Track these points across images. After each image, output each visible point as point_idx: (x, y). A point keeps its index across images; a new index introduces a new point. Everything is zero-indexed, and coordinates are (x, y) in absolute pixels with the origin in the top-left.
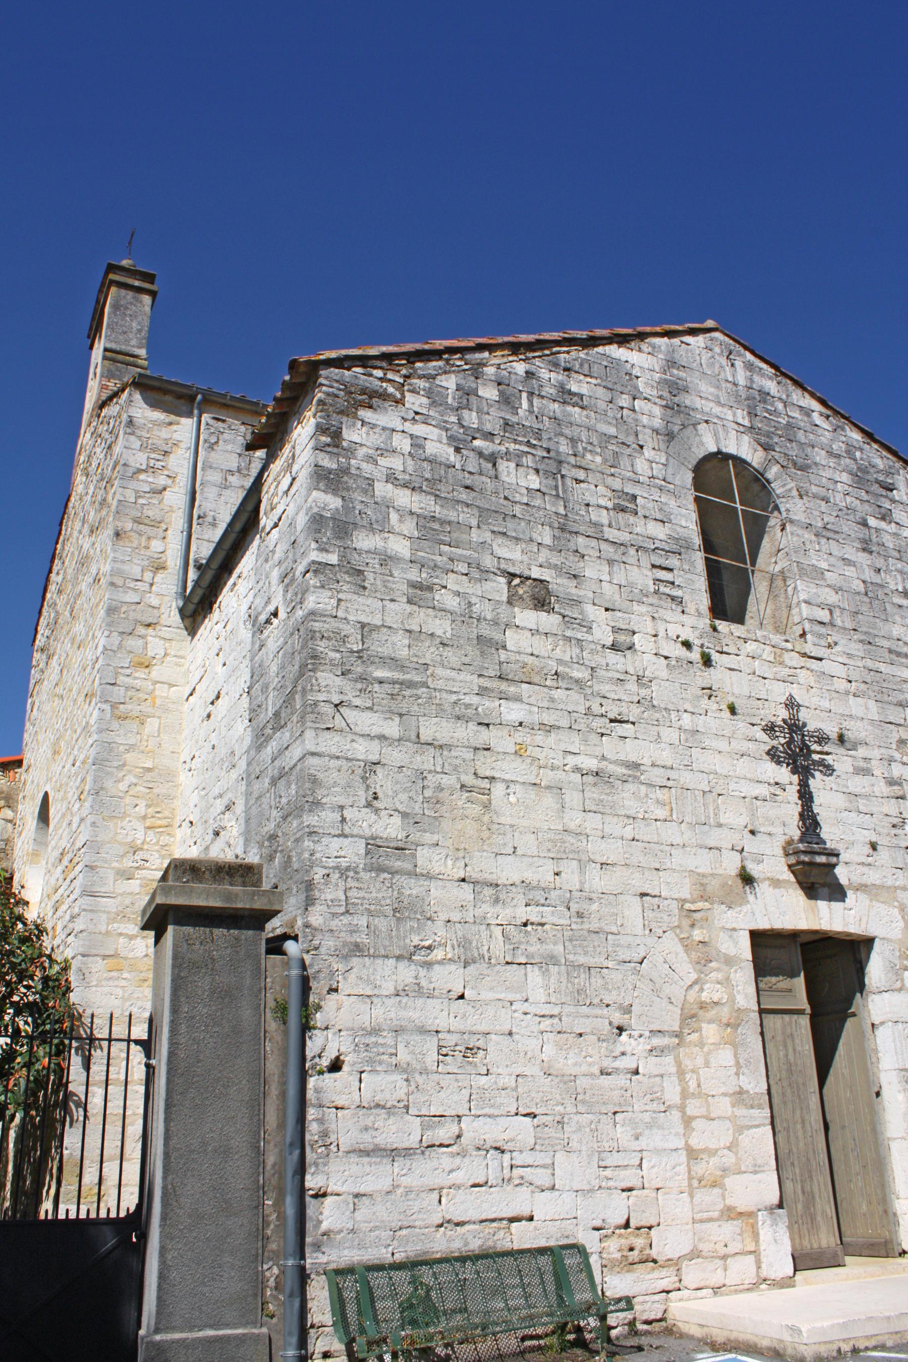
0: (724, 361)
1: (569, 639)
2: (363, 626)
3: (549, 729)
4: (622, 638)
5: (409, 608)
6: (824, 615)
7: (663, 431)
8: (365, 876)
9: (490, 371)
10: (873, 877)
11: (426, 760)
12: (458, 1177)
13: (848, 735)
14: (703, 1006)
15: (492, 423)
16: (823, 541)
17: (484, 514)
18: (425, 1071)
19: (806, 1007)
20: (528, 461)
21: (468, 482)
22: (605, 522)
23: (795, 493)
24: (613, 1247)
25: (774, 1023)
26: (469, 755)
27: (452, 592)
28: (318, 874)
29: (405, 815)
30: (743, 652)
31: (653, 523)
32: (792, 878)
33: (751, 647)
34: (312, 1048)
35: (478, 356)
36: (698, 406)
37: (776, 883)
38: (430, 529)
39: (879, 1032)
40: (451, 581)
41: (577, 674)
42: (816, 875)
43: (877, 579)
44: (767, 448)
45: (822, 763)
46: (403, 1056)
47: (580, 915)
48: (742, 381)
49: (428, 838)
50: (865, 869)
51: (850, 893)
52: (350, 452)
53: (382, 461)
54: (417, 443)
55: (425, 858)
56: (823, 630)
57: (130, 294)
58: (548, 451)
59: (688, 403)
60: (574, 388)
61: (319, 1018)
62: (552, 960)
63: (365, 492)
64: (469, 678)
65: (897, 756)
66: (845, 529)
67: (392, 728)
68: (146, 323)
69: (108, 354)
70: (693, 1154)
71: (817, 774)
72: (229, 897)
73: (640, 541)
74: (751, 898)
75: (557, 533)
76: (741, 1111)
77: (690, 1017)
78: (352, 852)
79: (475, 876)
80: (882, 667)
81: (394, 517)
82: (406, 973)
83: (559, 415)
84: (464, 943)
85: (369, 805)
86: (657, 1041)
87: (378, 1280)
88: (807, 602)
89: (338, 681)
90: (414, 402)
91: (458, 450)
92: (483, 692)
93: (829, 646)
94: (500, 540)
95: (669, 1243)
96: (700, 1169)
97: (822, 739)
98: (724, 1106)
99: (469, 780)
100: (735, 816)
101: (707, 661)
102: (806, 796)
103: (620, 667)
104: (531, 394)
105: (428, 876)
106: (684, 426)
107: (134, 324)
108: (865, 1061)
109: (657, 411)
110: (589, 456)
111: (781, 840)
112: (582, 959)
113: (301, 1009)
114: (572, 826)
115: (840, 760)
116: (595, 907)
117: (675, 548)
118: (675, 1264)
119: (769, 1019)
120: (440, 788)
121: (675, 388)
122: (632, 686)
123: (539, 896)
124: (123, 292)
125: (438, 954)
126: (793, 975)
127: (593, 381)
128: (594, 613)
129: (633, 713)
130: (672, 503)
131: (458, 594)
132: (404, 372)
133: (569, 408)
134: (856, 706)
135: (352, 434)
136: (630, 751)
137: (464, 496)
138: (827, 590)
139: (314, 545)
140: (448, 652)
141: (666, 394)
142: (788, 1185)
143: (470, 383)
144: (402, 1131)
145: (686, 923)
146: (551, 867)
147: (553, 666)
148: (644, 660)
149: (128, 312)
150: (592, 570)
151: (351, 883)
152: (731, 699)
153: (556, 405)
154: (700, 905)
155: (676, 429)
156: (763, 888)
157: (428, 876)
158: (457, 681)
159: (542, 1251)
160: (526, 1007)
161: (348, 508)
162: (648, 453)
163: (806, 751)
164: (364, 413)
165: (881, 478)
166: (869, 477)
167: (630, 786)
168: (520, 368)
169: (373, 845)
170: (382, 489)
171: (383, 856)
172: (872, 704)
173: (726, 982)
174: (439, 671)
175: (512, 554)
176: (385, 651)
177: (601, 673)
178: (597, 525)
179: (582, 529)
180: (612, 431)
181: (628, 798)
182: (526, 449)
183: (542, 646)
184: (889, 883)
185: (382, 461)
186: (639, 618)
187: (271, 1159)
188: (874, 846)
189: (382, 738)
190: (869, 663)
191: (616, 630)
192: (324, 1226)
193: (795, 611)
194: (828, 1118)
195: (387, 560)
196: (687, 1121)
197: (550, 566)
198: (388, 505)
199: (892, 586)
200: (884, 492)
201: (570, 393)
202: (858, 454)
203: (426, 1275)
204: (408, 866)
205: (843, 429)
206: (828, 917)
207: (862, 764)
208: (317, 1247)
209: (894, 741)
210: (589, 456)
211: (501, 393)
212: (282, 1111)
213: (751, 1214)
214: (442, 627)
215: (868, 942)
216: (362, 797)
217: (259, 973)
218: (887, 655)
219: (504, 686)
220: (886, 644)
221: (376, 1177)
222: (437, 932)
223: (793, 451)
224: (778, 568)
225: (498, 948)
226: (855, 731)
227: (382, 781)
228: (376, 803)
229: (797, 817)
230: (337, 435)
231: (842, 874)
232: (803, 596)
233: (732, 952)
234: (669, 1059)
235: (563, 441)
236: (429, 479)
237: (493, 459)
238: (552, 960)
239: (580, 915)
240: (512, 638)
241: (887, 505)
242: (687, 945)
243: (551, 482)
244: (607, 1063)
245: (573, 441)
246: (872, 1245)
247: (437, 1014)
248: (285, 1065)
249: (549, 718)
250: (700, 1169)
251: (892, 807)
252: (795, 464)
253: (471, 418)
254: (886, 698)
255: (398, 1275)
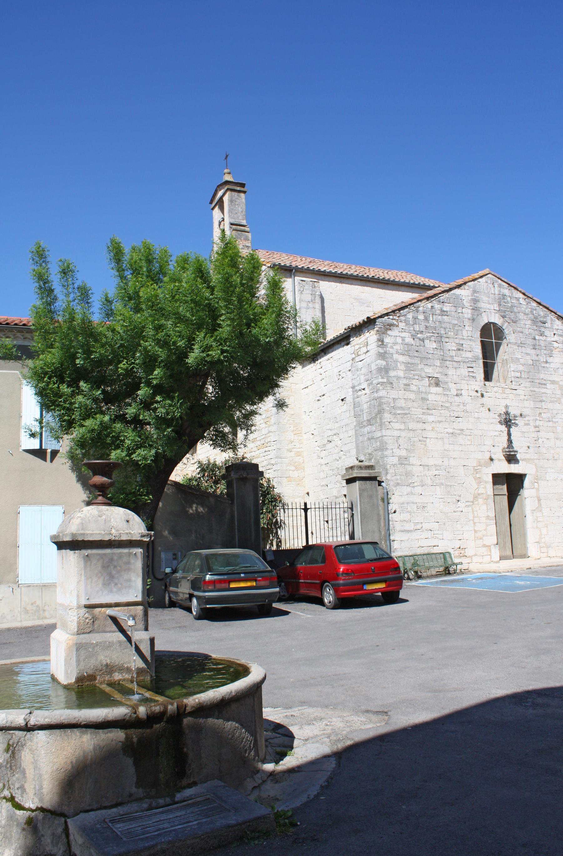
0: (491, 286)
1: (445, 395)
2: (394, 399)
3: (440, 422)
4: (459, 392)
5: (404, 392)
6: (518, 375)
7: (471, 319)
8: (399, 466)
9: (421, 309)
10: (527, 456)
11: (411, 434)
12: (422, 537)
13: (524, 413)
14: (479, 494)
15: (422, 328)
16: (520, 348)
17: (422, 359)
18: (414, 512)
19: (507, 493)
20: (433, 339)
21: (417, 350)
22: (454, 355)
23: (512, 332)
24: (457, 553)
25: (497, 498)
26: (420, 432)
27: (415, 384)
28: (388, 467)
29: (406, 449)
30: (493, 391)
31: (468, 353)
32: (504, 458)
33: (495, 389)
34: (390, 508)
35: (417, 304)
36: (482, 306)
37: (499, 460)
38: (409, 367)
39: (527, 500)
40: (414, 382)
41: (447, 405)
42: (511, 458)
43: (537, 358)
44: (503, 317)
45: (514, 423)
46: (409, 509)
47: (448, 472)
48: (497, 292)
49: (412, 455)
50: (525, 454)
51: (520, 462)
52: (386, 346)
53: (395, 347)
54: (403, 339)
55: (413, 460)
56: (517, 380)
57: (236, 194)
58: (438, 334)
59: (479, 306)
60: (445, 309)
61: (391, 501)
62: (442, 484)
63: (391, 358)
64: (420, 410)
65: (538, 418)
66: (528, 342)
67: (402, 427)
68: (244, 207)
69: (234, 227)
70: (476, 531)
71: (513, 427)
72: (370, 473)
73: (464, 360)
74: (492, 465)
75: (441, 361)
76: (488, 521)
77: (476, 497)
78: (395, 460)
79: (423, 464)
80: (536, 389)
81: (399, 364)
82: (409, 489)
83: (441, 320)
84: (422, 481)
85: (398, 448)
86: (468, 504)
87: (407, 559)
88: (513, 371)
89: (389, 415)
90: (402, 325)
91: (414, 339)
92: (423, 413)
93: (520, 385)
94: (426, 367)
95: (469, 552)
96: (477, 535)
97: (515, 416)
98: (483, 520)
99: (421, 438)
100: (489, 442)
101: (482, 396)
102: (509, 434)
103: (458, 401)
104: (433, 314)
105: (413, 465)
106: (478, 315)
107: (240, 209)
108: (522, 507)
109: (470, 311)
110: (449, 333)
111: (501, 448)
112: (449, 484)
113: (386, 500)
114: (446, 448)
115: (520, 421)
116: (452, 470)
117: (474, 360)
118: (471, 557)
119: (496, 497)
120: (414, 442)
121: (475, 301)
122: (461, 406)
123: (438, 468)
124: (233, 193)
125: (416, 484)
126: (503, 485)
127: (450, 305)
128: (451, 385)
129: (461, 414)
130: (474, 344)
131: (416, 386)
132: (398, 315)
133: (444, 317)
134: (526, 404)
135: (387, 340)
136: (461, 426)
137: (416, 354)
138: (520, 365)
139: (380, 377)
140: (414, 403)
141: (472, 304)
142: (499, 540)
143: (415, 315)
144: (408, 527)
145: (475, 472)
146: (441, 460)
147: (441, 403)
148: (465, 398)
149: (237, 203)
150: (451, 372)
151: (396, 468)
152: (489, 407)
153: (440, 317)
154: (479, 467)
155: (475, 317)
156: (495, 462)
157: (413, 465)
158: (417, 412)
159: (441, 553)
160: (436, 496)
161: (387, 364)
162: (467, 328)
163: (510, 420)
164: (389, 332)
165: (542, 319)
166: (538, 320)
167: (461, 436)
168: (429, 305)
169: (400, 458)
170: (396, 356)
171: (403, 461)
172: (532, 402)
173: (485, 488)
174: (412, 409)
175: (430, 371)
176: (399, 405)
177: (453, 404)
178: (452, 356)
179: (448, 359)
180: (456, 322)
181: (460, 439)
182: (432, 335)
183: (438, 398)
184: (532, 458)
185: (395, 347)
186: (463, 385)
187: (383, 533)
188: (529, 447)
189: (400, 429)
190: (532, 389)
191: (457, 390)
192: (395, 547)
193: (509, 373)
194: (512, 523)
195: (398, 378)
196: (474, 523)
197: (440, 373)
198: (396, 361)
199: (542, 360)
200: (542, 325)
201: (444, 311)
202: (534, 312)
203: (416, 558)
204: (408, 463)
205: (530, 303)
206: (514, 469)
207: (527, 422)
208: (394, 552)
209: (537, 414)
210: (449, 333)
211: (425, 316)
212: (385, 522)
213: (490, 546)
214: (412, 396)
215: (525, 475)
216: (397, 445)
217: (377, 491)
218: (538, 385)
219: (428, 411)
220: (538, 381)
221: (405, 537)
222: (415, 479)
223: (512, 316)
224: (505, 358)
225: (429, 482)
226: (525, 412)
227: (401, 441)
228: (400, 447)
229: (506, 441)
230: (382, 341)
231: (518, 456)
232: (512, 369)
233: (487, 480)
234: (470, 508)
235: (442, 329)
236: (407, 351)
237: (423, 340)
238: (442, 484)
239: (448, 472)
240: (430, 397)
241: (543, 329)
242: (475, 479)
243: (439, 345)
244: (456, 510)
245: (445, 328)
246: (521, 556)
247: (417, 499)
248: (385, 512)
249: (440, 419)
250: (477, 535)
251: (535, 435)
252: (513, 321)
253: (417, 328)
254: (536, 400)
255: (411, 558)
